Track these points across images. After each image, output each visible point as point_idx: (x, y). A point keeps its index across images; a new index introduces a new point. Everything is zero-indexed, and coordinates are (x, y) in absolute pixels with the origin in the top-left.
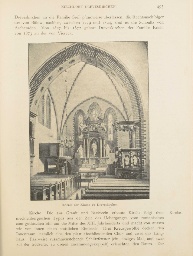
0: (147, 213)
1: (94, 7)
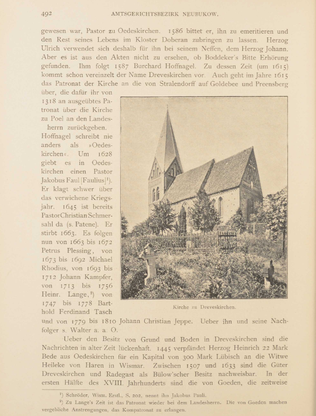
0: (99, 67)
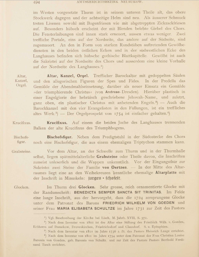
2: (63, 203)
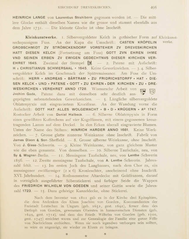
1: (90, 8)
2: (95, 74)
